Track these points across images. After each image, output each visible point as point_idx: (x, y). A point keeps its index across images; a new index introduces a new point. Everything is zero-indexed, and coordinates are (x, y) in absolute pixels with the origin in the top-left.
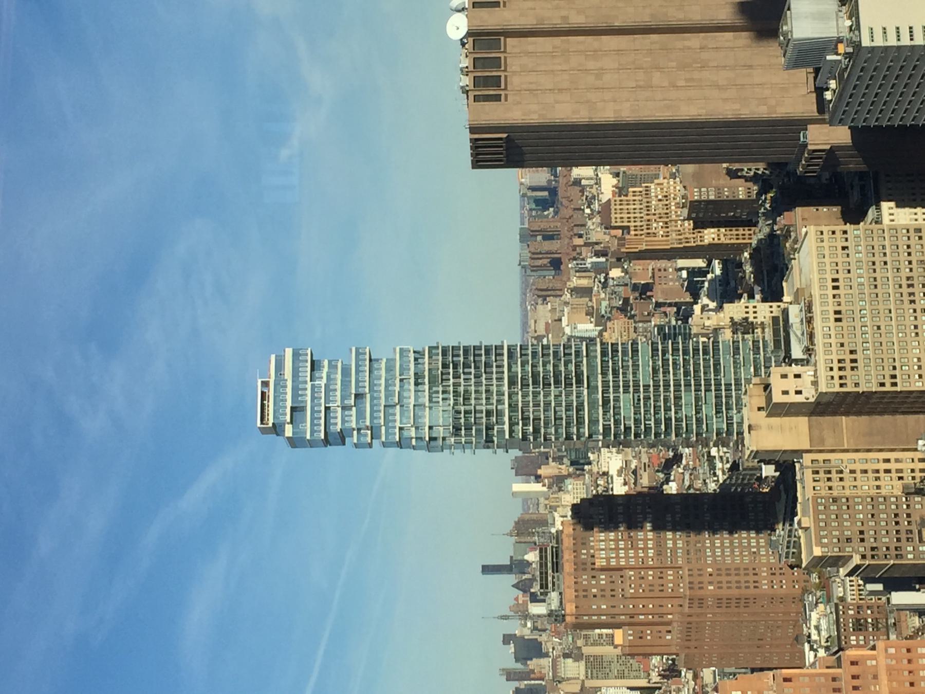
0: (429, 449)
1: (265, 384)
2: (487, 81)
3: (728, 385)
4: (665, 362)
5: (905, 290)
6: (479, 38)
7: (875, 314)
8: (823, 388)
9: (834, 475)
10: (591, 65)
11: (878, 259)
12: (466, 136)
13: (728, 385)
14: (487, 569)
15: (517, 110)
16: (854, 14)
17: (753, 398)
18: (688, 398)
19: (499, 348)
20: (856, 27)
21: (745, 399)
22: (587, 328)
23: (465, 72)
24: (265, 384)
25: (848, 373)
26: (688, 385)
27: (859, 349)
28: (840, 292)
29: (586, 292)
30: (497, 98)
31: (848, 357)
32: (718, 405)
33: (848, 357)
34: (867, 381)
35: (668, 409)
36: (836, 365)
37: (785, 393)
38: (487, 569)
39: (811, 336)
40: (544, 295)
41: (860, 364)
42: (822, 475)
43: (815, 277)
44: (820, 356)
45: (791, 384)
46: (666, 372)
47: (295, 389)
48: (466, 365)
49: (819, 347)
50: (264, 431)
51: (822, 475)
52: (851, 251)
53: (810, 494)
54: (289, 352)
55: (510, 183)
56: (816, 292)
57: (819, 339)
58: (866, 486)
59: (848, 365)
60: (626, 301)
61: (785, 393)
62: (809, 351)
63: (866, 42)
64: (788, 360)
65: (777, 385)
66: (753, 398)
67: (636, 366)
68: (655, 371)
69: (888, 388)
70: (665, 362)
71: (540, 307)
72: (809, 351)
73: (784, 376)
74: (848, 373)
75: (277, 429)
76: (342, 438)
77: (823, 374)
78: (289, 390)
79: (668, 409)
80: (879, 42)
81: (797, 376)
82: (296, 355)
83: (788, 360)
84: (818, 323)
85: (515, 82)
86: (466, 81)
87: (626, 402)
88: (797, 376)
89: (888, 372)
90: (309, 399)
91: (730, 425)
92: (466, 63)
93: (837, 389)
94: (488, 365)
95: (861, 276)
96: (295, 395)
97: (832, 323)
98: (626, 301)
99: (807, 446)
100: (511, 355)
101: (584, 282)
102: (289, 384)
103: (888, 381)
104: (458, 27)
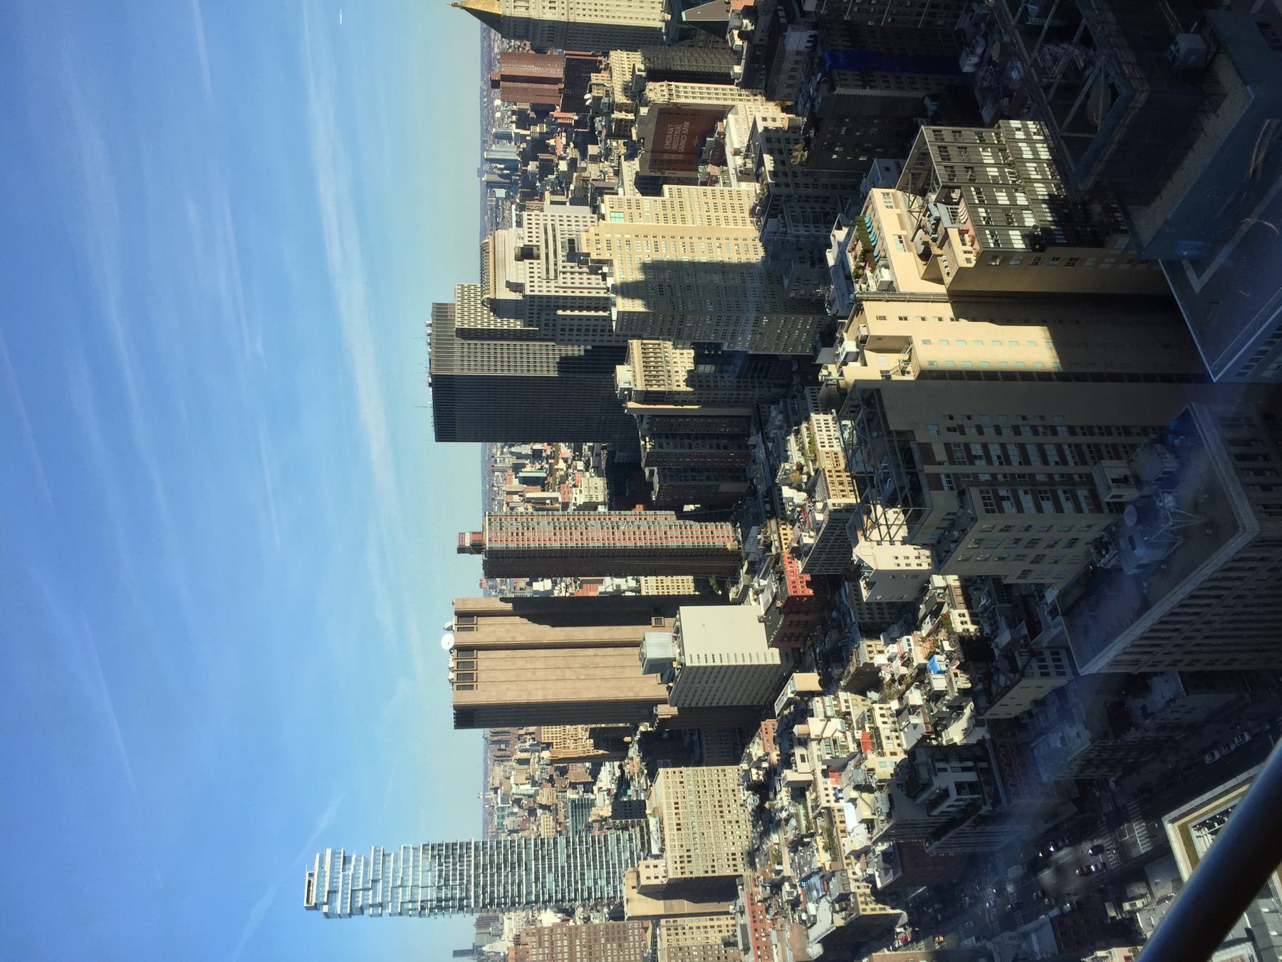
0: (420, 915)
1: (311, 875)
2: (465, 678)
3: (614, 865)
4: (574, 849)
5: (718, 809)
6: (462, 650)
7: (701, 824)
8: (671, 876)
9: (680, 931)
10: (529, 666)
11: (701, 789)
12: (452, 711)
13: (614, 865)
14: (457, 953)
15: (480, 696)
16: (681, 645)
17: (630, 880)
18: (589, 874)
19: (468, 844)
20: (682, 654)
21: (624, 880)
22: (528, 789)
23: (451, 669)
24: (311, 875)
25: (686, 864)
26: (589, 865)
27: (692, 849)
28: (680, 811)
29: (525, 762)
30: (471, 687)
31: (686, 854)
32: (608, 878)
33: (686, 854)
34: (698, 870)
35: (576, 883)
36: (678, 860)
37: (648, 878)
38: (457, 953)
39: (663, 841)
40: (501, 759)
41: (693, 859)
42: (672, 931)
43: (664, 802)
44: (668, 854)
45: (652, 872)
46: (575, 857)
47: (331, 878)
48: (447, 857)
49: (668, 848)
50: (308, 908)
51: (672, 931)
52: (685, 784)
53: (665, 945)
54: (329, 851)
55: (477, 736)
56: (665, 812)
57: (667, 843)
58: (699, 937)
59: (686, 859)
60: (551, 776)
61: (648, 878)
62: (662, 850)
63: (688, 664)
64: (649, 854)
65: (644, 873)
66: (630, 880)
67: (556, 852)
68: (568, 856)
69: (710, 874)
70: (574, 849)
71: (497, 768)
72: (662, 850)
73: (648, 867)
74: (686, 864)
75: (316, 907)
76: (362, 910)
77: (671, 866)
78: (327, 879)
79: (576, 883)
80: (696, 664)
81: (656, 866)
82: (333, 853)
83: (649, 854)
84: (666, 832)
85: (482, 676)
86: (452, 676)
87: (550, 878)
88: (656, 866)
89: (710, 864)
90: (340, 885)
91: (615, 892)
92: (452, 664)
93: (679, 876)
94: (461, 856)
95: (692, 799)
96: (331, 882)
97: (675, 832)
98: (551, 776)
99: (662, 912)
100: (476, 848)
101: (525, 755)
102: (328, 874)
103: (710, 869)
104: (448, 641)
